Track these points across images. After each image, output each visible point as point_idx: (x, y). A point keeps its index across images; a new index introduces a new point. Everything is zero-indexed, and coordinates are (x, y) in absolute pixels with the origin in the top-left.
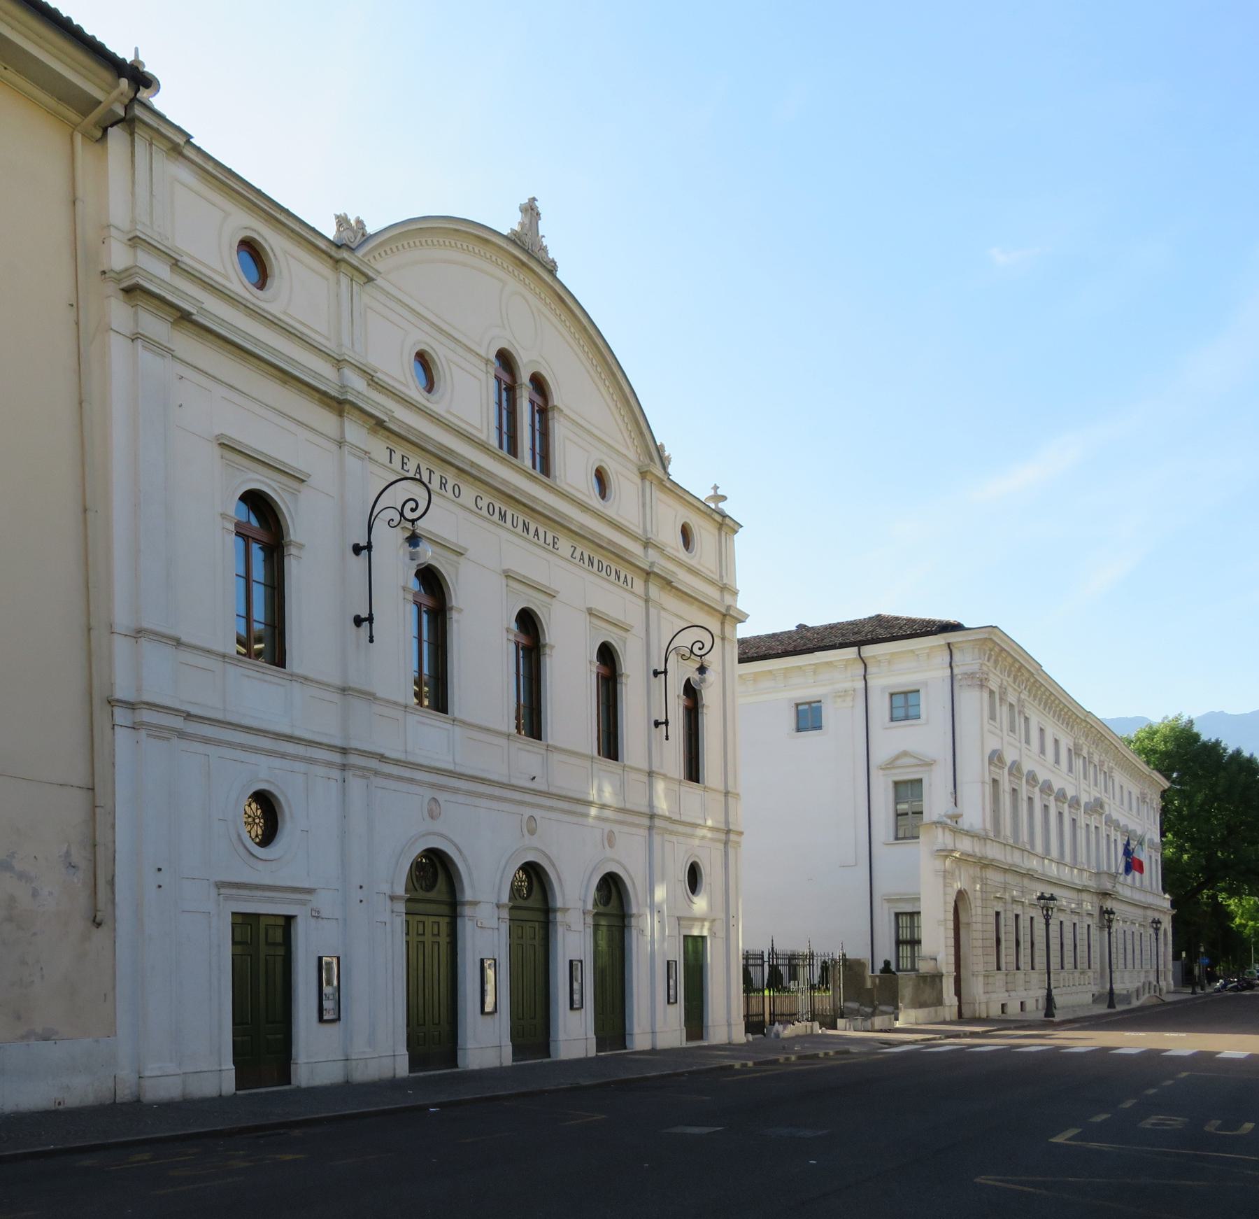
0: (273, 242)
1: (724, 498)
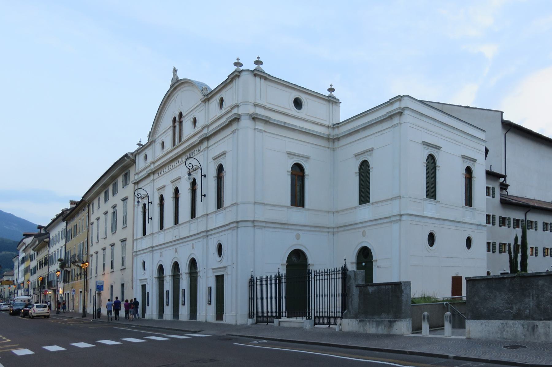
0: (303, 97)
1: (261, 63)
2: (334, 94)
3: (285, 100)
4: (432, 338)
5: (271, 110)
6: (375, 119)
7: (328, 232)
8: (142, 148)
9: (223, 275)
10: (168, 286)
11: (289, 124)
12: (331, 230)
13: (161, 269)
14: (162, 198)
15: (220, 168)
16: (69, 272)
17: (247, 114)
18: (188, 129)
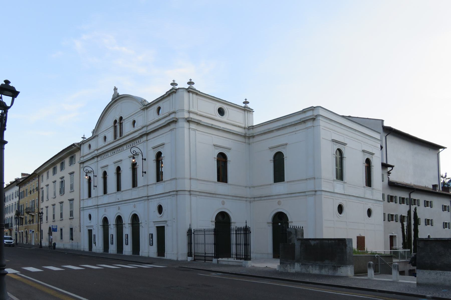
0: (225, 107)
2: (248, 105)
3: (211, 109)
4: (355, 279)
5: (201, 115)
6: (289, 123)
7: (246, 201)
8: (85, 141)
9: (164, 227)
10: (112, 231)
11: (215, 126)
12: (248, 199)
13: (105, 220)
14: (105, 173)
15: (159, 155)
16: (23, 218)
17: (184, 118)
18: (127, 128)
